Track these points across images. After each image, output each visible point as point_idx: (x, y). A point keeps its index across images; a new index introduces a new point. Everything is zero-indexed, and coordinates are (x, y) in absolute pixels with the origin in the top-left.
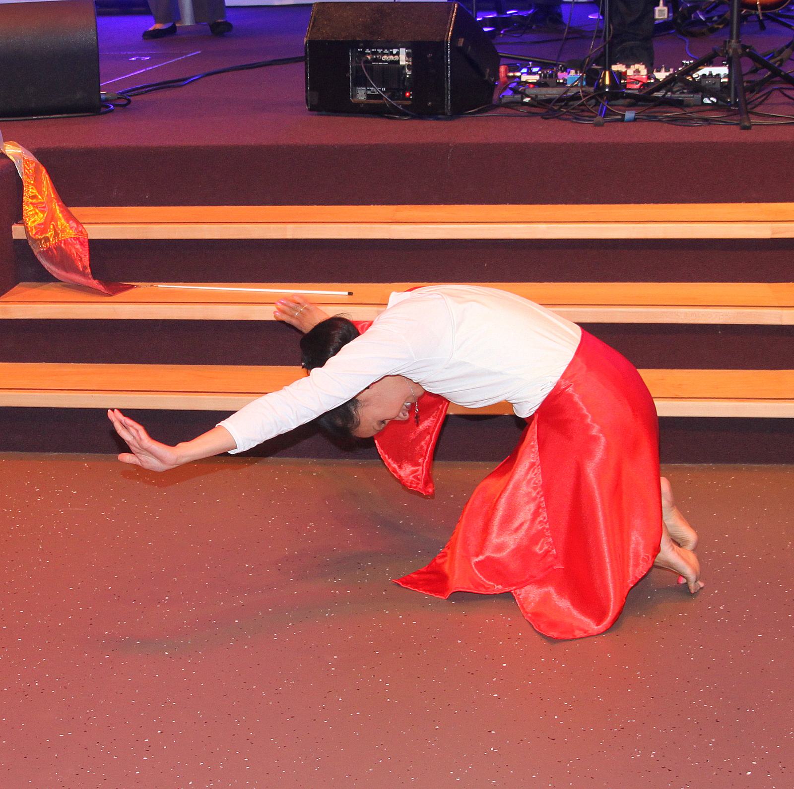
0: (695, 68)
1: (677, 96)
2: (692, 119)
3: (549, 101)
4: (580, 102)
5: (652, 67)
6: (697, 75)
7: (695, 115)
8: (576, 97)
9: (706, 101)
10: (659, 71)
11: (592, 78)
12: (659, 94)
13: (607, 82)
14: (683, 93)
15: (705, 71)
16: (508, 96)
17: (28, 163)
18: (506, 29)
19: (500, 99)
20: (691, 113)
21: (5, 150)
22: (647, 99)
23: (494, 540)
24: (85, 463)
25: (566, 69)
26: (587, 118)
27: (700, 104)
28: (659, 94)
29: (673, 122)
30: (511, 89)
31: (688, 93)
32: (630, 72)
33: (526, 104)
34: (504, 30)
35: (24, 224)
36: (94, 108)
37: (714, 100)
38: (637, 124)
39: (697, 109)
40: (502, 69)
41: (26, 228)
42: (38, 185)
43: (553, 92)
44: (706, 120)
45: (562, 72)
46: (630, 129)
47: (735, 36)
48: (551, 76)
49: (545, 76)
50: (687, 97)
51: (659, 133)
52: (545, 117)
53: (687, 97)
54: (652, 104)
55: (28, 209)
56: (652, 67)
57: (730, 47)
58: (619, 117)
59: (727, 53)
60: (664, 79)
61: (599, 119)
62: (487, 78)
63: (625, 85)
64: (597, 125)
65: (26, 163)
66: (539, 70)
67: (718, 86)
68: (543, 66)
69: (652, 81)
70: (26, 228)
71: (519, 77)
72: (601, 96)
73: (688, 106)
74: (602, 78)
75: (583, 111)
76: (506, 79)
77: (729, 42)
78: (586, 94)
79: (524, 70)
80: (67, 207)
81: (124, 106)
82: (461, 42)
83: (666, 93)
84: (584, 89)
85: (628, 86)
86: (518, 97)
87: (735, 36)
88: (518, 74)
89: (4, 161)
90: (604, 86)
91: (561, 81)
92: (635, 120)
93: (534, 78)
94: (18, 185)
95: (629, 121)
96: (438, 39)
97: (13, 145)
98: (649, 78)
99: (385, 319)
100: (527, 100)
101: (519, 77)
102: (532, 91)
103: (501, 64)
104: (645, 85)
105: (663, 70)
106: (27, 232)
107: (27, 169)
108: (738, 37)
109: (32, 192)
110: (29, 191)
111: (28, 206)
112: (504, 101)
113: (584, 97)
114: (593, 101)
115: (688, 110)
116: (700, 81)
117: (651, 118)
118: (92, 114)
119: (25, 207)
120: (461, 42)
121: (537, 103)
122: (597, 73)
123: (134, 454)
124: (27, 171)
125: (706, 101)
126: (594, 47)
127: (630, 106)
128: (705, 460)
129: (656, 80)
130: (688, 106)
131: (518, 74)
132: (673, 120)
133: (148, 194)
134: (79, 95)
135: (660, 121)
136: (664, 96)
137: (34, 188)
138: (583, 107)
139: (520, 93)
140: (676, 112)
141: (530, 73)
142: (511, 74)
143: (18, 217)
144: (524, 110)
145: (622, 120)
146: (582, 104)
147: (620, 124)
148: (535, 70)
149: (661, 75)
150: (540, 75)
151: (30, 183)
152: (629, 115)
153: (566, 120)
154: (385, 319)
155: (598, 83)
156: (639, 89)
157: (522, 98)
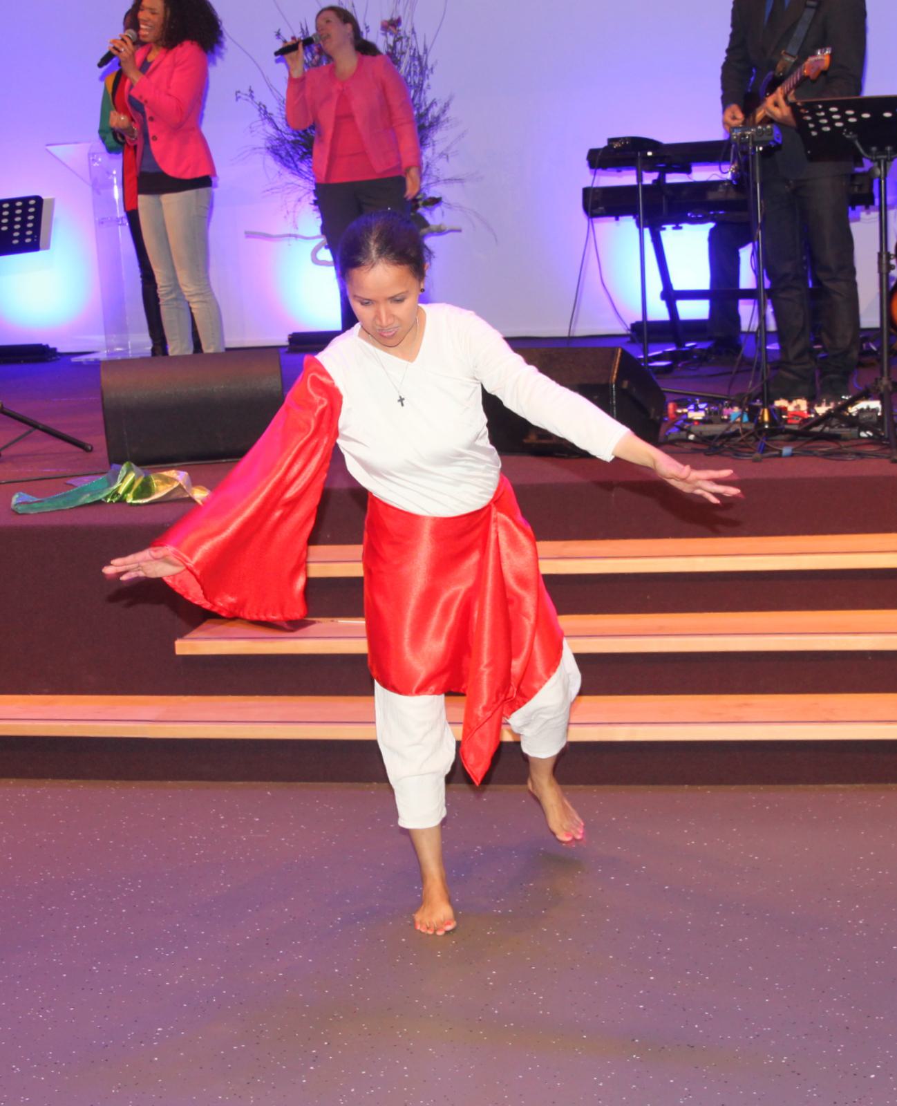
0: (852, 402)
1: (836, 430)
2: (846, 453)
3: (712, 438)
4: (739, 439)
5: (813, 401)
6: (853, 410)
7: (850, 449)
8: (736, 434)
9: (863, 434)
10: (819, 405)
11: (753, 414)
12: (817, 429)
13: (766, 418)
14: (841, 427)
15: (863, 405)
16: (674, 433)
18: (685, 362)
19: (667, 437)
20: (847, 447)
21: (193, 494)
22: (806, 433)
25: (731, 406)
26: (746, 454)
27: (857, 437)
28: (817, 429)
29: (829, 457)
30: (677, 427)
31: (847, 427)
32: (791, 408)
33: (690, 441)
34: (683, 363)
37: (870, 434)
38: (793, 459)
39: (855, 442)
40: (671, 406)
43: (717, 429)
44: (858, 454)
45: (728, 408)
46: (787, 462)
47: (886, 374)
48: (716, 413)
49: (710, 413)
50: (844, 431)
51: (815, 468)
52: (706, 453)
53: (844, 431)
54: (810, 438)
56: (813, 401)
57: (881, 384)
58: (777, 453)
59: (878, 390)
60: (823, 414)
61: (757, 455)
62: (652, 417)
63: (786, 421)
64: (755, 461)
66: (706, 407)
67: (875, 419)
68: (710, 401)
69: (813, 416)
71: (686, 414)
72: (760, 433)
73: (845, 440)
75: (742, 447)
76: (674, 416)
77: (881, 379)
78: (745, 431)
79: (692, 407)
82: (625, 384)
83: (824, 428)
84: (744, 426)
85: (789, 421)
86: (683, 434)
87: (886, 374)
88: (685, 410)
90: (763, 423)
91: (726, 417)
92: (792, 455)
93: (699, 416)
95: (787, 456)
96: (604, 382)
97: (202, 489)
98: (809, 412)
99: (414, 483)
100: (691, 437)
101: (686, 414)
102: (696, 428)
103: (667, 400)
104: (805, 420)
105: (824, 404)
108: (889, 375)
112: (671, 438)
113: (744, 433)
114: (752, 438)
115: (843, 444)
116: (857, 416)
117: (809, 453)
120: (625, 384)
121: (703, 439)
122: (757, 409)
123: (482, 385)
125: (863, 434)
126: (753, 385)
127: (789, 441)
128: (857, 780)
129: (816, 414)
130: (845, 440)
131: (685, 410)
132: (827, 455)
135: (815, 455)
136: (822, 430)
138: (743, 444)
139: (686, 430)
140: (830, 446)
141: (697, 409)
142: (679, 411)
144: (687, 447)
145: (780, 455)
146: (742, 440)
147: (777, 461)
148: (702, 406)
149: (821, 410)
150: (706, 412)
152: (787, 450)
153: (727, 456)
154: (414, 483)
155: (758, 420)
156: (800, 424)
157: (688, 435)
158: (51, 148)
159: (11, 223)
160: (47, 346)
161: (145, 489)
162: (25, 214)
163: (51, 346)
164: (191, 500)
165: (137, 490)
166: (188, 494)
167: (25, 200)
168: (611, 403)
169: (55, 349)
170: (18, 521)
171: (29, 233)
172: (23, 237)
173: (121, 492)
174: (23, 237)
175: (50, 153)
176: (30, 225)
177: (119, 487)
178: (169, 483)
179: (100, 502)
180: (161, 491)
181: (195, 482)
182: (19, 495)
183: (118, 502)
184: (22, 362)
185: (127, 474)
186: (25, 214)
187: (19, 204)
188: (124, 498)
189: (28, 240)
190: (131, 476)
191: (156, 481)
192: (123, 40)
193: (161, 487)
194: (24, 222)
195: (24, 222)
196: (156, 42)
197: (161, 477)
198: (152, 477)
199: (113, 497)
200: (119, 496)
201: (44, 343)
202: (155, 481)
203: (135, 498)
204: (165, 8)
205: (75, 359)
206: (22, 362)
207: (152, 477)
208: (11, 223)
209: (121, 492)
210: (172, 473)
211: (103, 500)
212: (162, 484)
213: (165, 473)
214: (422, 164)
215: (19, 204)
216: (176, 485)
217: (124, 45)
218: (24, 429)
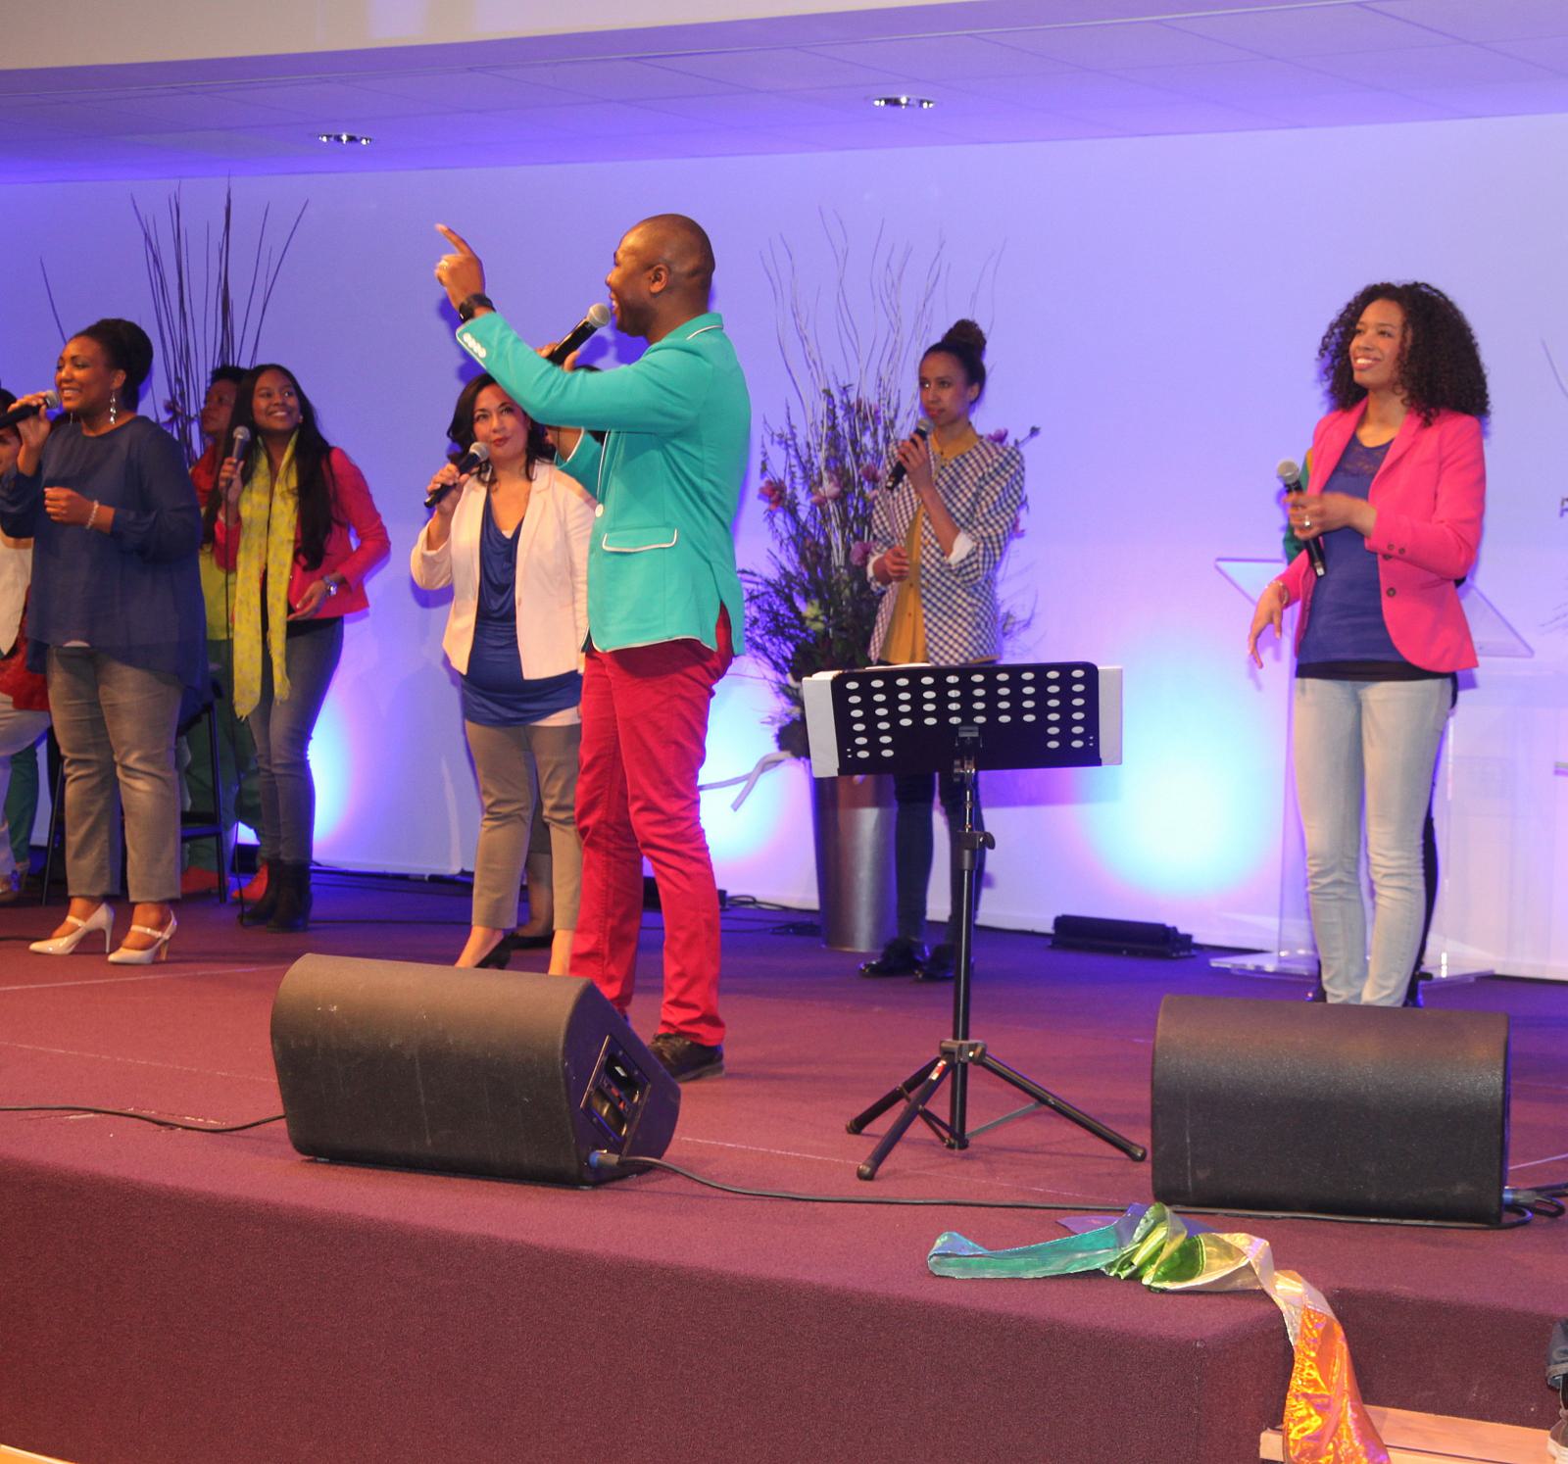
17: (1312, 1316)
23: (873, 584)
24: (1314, 993)
35: (1285, 1433)
36: (1489, 1215)
41: (1286, 1440)
42: (1323, 1363)
55: (1296, 1407)
65: (1309, 1317)
70: (1286, 1440)
74: (206, 1120)
80: (1366, 1402)
81: (1553, 1216)
89: (1264, 1307)
94: (1286, 1358)
106: (1286, 1449)
107: (1307, 1328)
109: (1309, 1374)
110: (1305, 1372)
111: (1297, 1400)
118: (764, 906)
119: (1291, 1401)
124: (1307, 1331)
133: (1534, 1404)
134: (1460, 1189)
137: (1314, 1365)
143: (1275, 1418)
151: (1308, 1357)
158: (1224, 565)
159: (1041, 710)
160: (1175, 929)
161: (1187, 1261)
162: (1066, 695)
163: (1182, 930)
164: (1264, 1296)
165: (1171, 1258)
166: (1260, 1284)
167: (1065, 669)
168: (1330, 1378)
169: (1189, 937)
170: (927, 1292)
171: (1078, 730)
172: (1066, 737)
173: (1137, 1261)
174: (1066, 737)
175: (1221, 572)
176: (1078, 716)
177: (1135, 1252)
178: (1232, 1258)
179: (1097, 1273)
180: (1212, 1271)
181: (1282, 1260)
182: (950, 1236)
183: (1129, 1278)
184: (1125, 952)
185: (1154, 1227)
186: (1066, 695)
187: (1053, 675)
188: (1141, 1273)
189: (1077, 744)
190: (1160, 1233)
191: (1209, 1249)
192: (913, 440)
193: (1216, 1262)
194: (1066, 709)
195: (1066, 709)
196: (1390, 386)
197: (1218, 1243)
198: (1202, 1238)
199: (1121, 1269)
200: (1134, 1268)
201: (1169, 923)
202: (1207, 1248)
203: (1165, 1277)
204: (1405, 325)
205: (1215, 963)
206: (1125, 952)
207: (1202, 1238)
208: (1041, 710)
209: (1137, 1261)
210: (1239, 1240)
211: (1103, 1269)
212: (1219, 1257)
213: (1226, 1237)
214: (943, 803)
215: (1053, 675)
216: (1243, 1263)
217: (914, 450)
218: (1031, 1104)
